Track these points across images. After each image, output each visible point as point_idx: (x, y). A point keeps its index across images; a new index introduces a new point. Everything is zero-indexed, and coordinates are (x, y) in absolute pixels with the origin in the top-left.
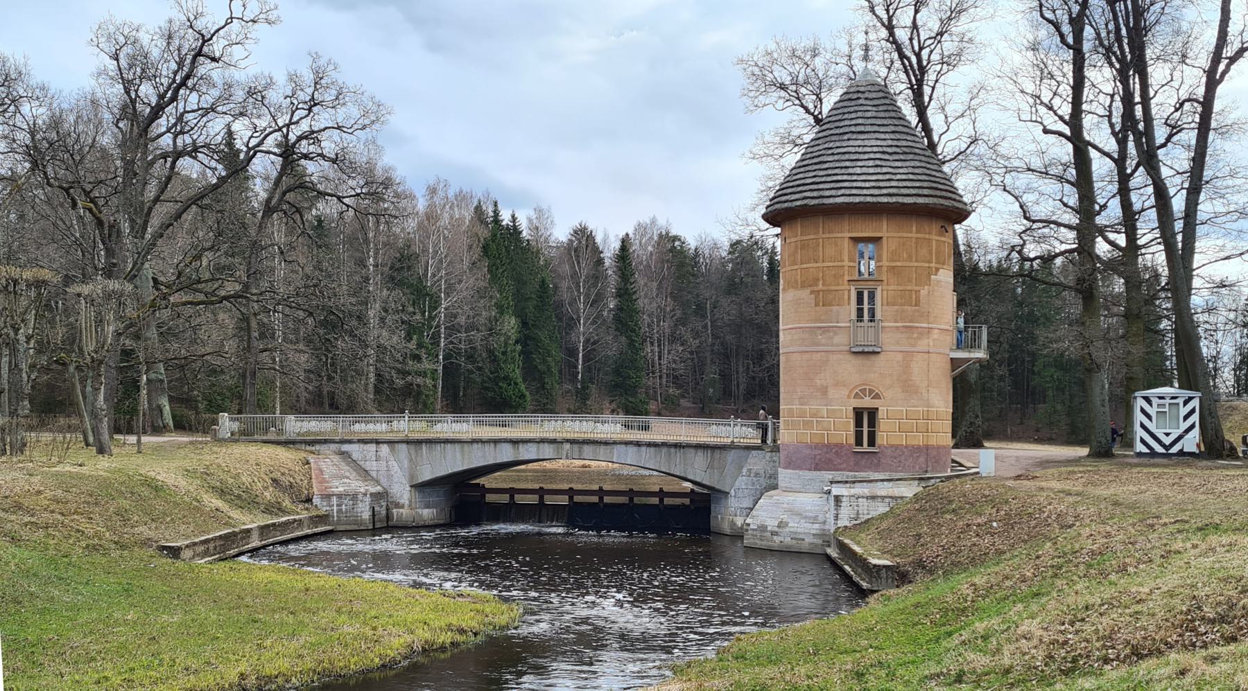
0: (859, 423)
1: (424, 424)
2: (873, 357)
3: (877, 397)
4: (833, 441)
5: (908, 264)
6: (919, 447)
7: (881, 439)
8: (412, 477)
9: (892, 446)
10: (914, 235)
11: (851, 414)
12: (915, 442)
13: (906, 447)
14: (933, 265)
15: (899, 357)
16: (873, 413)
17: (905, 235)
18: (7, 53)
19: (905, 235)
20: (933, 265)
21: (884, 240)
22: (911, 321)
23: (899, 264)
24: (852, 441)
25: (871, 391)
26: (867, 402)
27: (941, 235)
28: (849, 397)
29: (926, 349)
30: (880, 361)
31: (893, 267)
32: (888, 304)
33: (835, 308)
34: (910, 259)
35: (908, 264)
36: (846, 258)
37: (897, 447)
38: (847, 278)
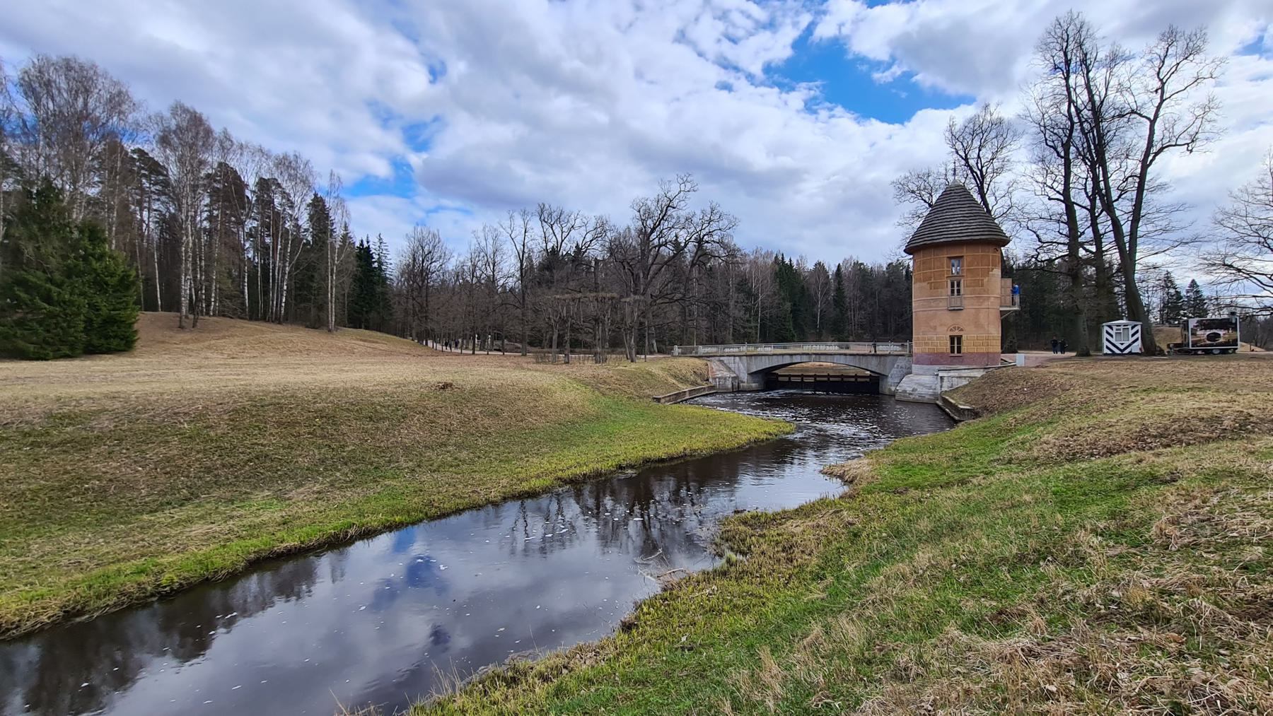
0: (952, 342)
7: (964, 349)
16: (959, 338)
26: (956, 333)
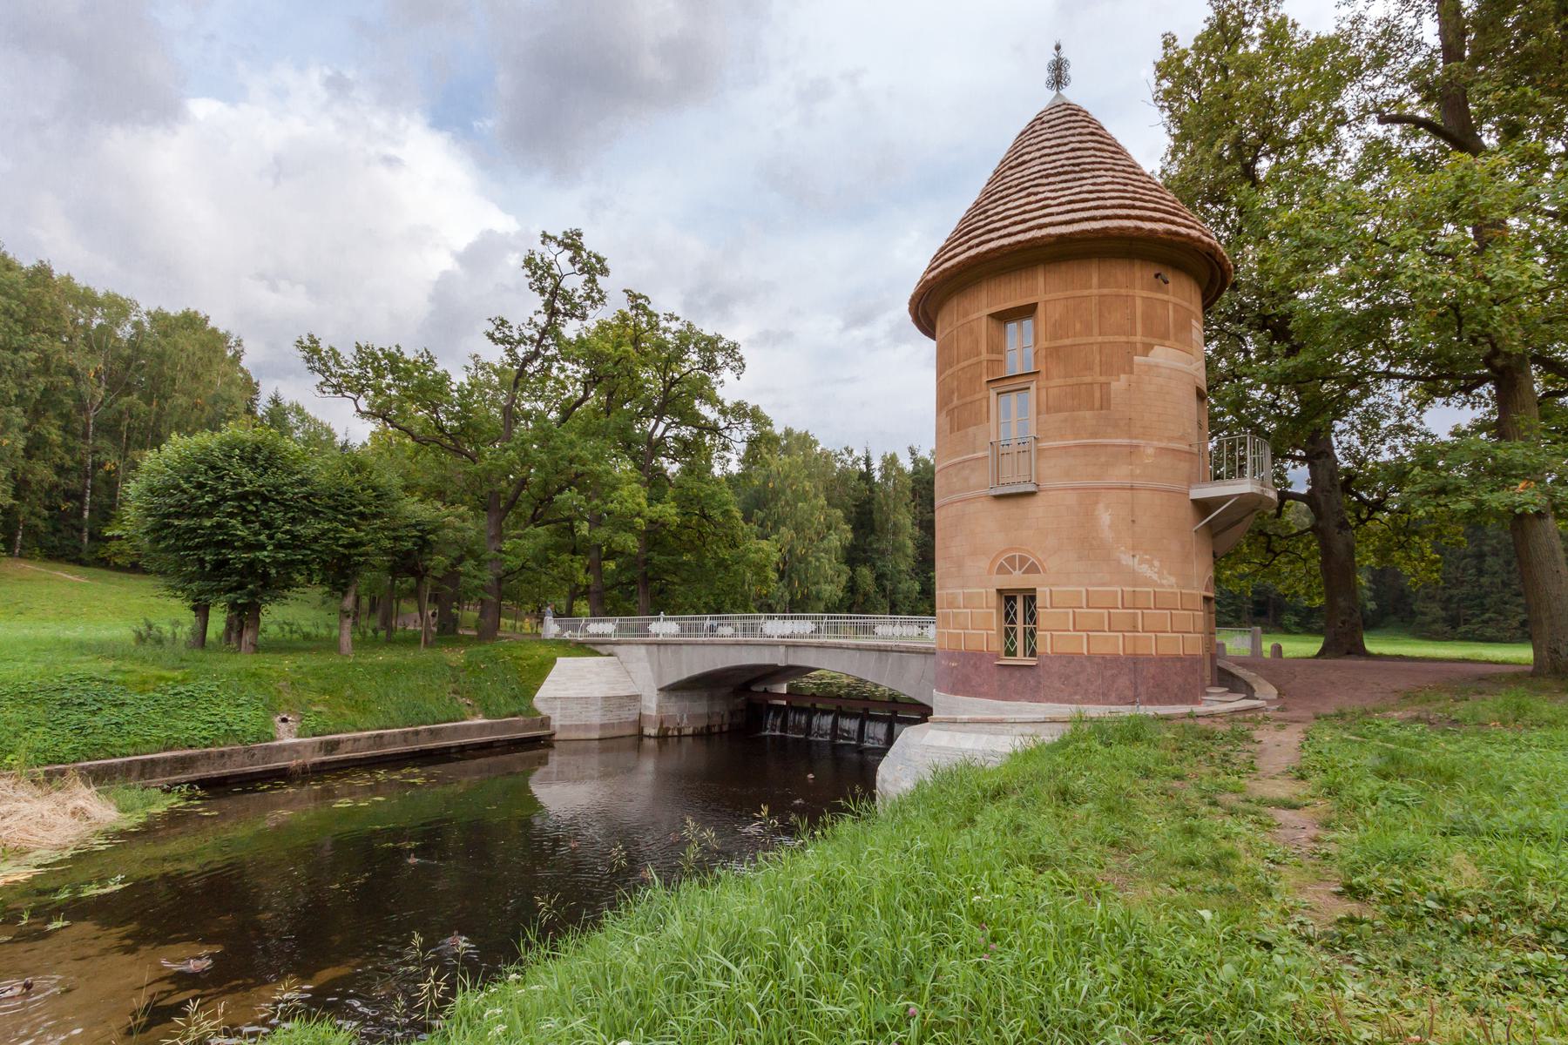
0: (1009, 616)
1: (916, 630)
2: (1025, 502)
3: (1033, 569)
4: (972, 646)
5: (1084, 340)
6: (1116, 659)
7: (1046, 642)
8: (659, 677)
9: (1061, 656)
10: (1095, 291)
11: (993, 599)
12: (1106, 649)
13: (1090, 657)
14: (1138, 338)
15: (1071, 499)
16: (1030, 598)
17: (1078, 293)
18: (59, 246)
19: (1078, 293)
20: (1138, 338)
21: (1040, 308)
22: (1094, 435)
23: (1067, 342)
24: (997, 645)
25: (1023, 560)
26: (1017, 580)
27: (1159, 289)
28: (990, 572)
29: (1127, 482)
30: (1036, 509)
31: (1057, 349)
32: (1048, 410)
33: (971, 430)
34: (1088, 330)
35: (1084, 340)
36: (984, 350)
37: (1070, 658)
38: (985, 379)
